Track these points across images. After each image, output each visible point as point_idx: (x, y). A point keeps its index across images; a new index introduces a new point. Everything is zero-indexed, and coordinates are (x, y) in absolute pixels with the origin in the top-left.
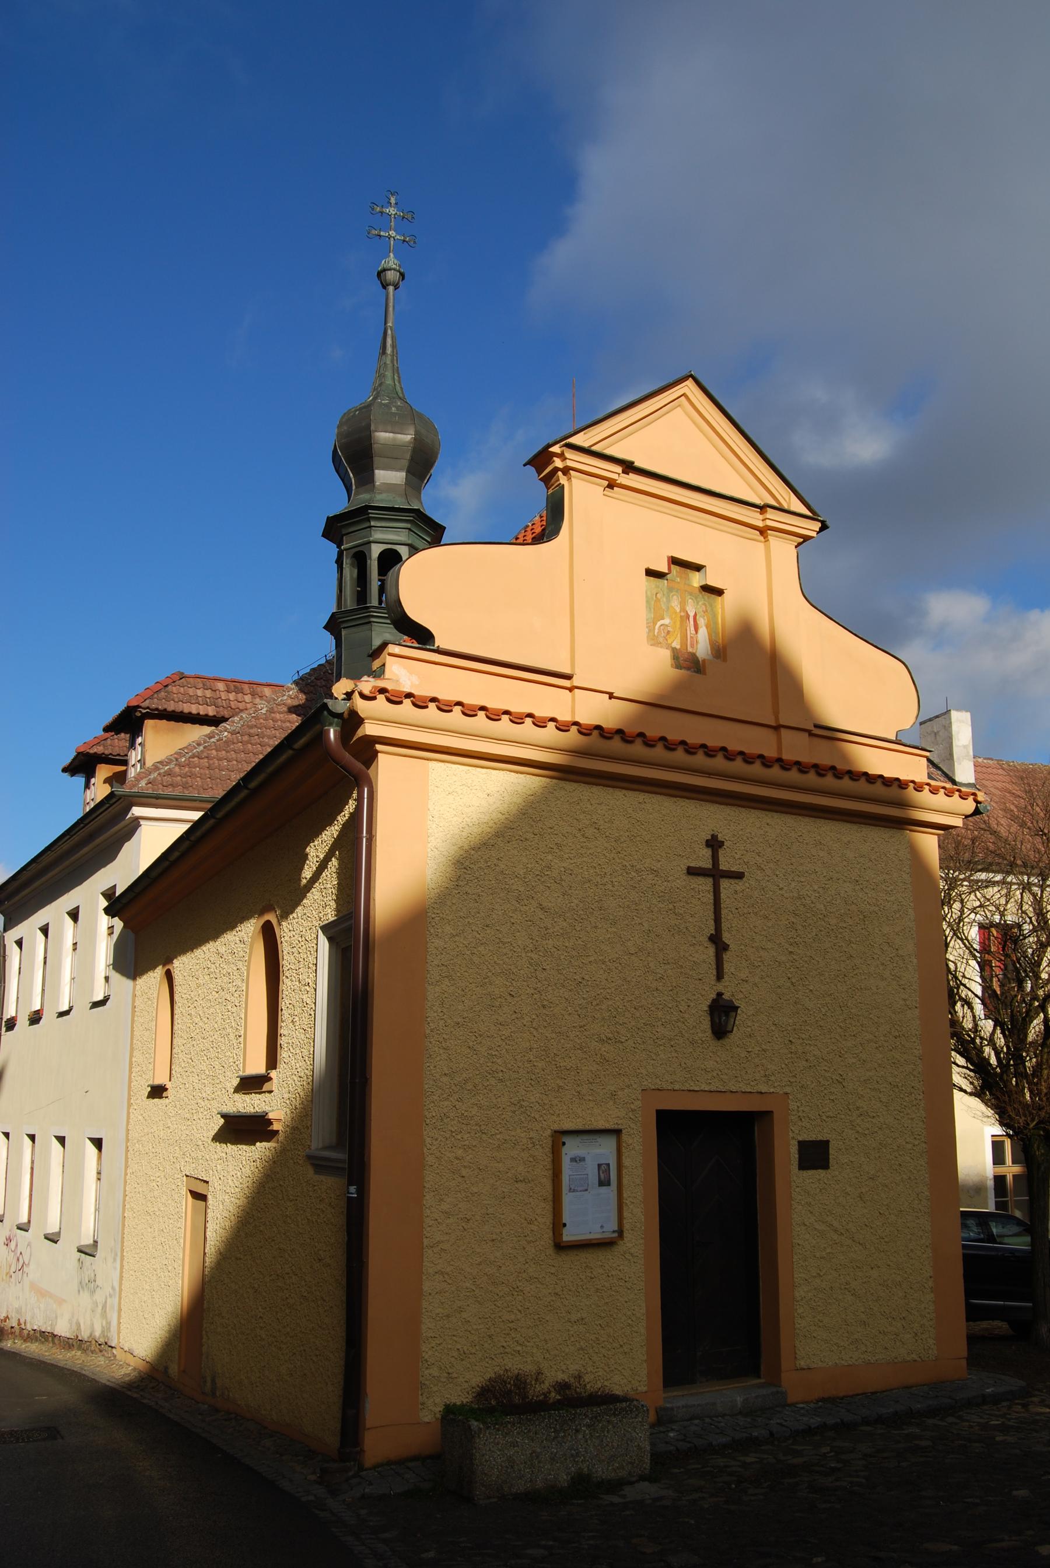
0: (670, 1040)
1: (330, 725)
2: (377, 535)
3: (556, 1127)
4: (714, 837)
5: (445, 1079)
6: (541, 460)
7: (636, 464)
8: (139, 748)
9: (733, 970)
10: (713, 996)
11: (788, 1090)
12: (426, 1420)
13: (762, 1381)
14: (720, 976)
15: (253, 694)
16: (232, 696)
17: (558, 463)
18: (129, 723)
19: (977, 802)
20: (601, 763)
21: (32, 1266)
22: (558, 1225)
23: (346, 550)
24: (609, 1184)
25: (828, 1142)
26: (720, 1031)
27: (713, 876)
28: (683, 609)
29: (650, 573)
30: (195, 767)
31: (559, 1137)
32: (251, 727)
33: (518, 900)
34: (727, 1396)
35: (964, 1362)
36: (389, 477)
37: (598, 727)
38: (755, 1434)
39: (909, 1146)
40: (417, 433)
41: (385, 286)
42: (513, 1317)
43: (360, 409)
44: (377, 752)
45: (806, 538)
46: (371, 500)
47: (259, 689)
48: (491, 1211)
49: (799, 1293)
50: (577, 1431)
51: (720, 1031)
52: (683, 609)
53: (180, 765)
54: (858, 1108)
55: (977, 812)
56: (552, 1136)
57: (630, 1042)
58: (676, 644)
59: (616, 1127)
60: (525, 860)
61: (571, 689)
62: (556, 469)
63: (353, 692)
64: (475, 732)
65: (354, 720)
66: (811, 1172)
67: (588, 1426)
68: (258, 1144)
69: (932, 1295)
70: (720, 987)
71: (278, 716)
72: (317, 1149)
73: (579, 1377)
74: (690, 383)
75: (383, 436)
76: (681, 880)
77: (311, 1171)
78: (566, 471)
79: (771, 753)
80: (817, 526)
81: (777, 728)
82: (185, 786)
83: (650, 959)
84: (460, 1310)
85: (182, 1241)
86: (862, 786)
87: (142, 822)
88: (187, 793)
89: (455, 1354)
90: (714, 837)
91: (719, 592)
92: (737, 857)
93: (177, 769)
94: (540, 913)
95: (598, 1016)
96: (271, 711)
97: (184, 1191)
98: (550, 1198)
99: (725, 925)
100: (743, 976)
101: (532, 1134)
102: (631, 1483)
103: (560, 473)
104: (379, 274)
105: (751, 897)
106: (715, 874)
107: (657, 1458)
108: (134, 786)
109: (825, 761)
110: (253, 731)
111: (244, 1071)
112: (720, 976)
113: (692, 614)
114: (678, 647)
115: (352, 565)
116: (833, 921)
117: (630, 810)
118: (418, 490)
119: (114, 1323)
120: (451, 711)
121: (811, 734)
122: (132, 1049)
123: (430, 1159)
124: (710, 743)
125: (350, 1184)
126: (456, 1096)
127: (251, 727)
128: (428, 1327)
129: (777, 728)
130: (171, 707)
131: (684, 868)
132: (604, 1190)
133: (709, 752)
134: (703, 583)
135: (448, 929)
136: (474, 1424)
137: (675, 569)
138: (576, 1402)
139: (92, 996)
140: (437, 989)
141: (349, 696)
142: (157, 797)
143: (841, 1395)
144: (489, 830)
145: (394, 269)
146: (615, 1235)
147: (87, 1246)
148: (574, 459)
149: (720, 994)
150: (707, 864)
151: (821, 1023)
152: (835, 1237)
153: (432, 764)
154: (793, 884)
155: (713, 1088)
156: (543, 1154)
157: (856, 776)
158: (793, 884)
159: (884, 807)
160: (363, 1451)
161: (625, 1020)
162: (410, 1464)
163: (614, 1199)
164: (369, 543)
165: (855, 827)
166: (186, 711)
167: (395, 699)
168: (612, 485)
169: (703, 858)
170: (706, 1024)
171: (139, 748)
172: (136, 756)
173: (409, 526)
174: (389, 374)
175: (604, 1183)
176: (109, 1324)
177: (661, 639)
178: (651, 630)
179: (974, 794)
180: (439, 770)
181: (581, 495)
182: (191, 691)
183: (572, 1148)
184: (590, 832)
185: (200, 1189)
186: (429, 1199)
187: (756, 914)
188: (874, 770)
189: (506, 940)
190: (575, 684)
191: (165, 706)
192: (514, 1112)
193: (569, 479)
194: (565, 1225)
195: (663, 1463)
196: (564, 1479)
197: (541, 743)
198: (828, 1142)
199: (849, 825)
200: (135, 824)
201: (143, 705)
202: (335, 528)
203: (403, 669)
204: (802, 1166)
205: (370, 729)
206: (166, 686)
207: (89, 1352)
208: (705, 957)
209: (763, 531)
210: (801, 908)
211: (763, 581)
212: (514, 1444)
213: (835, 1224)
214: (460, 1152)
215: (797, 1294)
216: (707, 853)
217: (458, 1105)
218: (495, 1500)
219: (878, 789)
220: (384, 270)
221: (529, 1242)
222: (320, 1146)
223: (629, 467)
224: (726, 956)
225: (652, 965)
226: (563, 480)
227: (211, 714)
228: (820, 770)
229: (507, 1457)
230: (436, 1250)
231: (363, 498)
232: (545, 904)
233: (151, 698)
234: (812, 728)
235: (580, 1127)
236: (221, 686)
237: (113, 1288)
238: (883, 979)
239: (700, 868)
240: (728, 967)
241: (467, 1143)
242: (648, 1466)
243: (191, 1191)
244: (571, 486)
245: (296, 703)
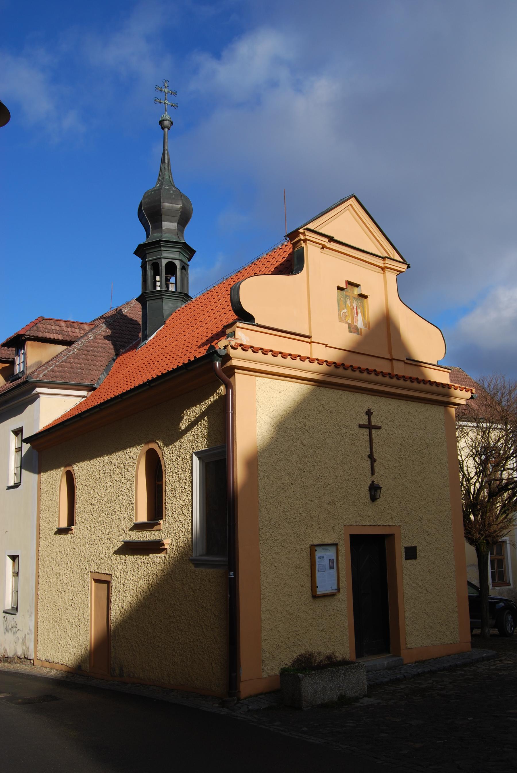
0: (354, 502)
1: (217, 360)
2: (164, 255)
3: (311, 543)
4: (369, 410)
5: (267, 523)
6: (293, 235)
7: (335, 238)
8: (22, 356)
9: (378, 471)
10: (370, 482)
11: (400, 524)
12: (265, 676)
13: (390, 655)
14: (373, 473)
15: (80, 329)
16: (69, 329)
17: (302, 237)
18: (17, 342)
19: (472, 393)
20: (340, 378)
22: (314, 586)
23: (148, 261)
24: (333, 568)
25: (416, 547)
26: (374, 498)
27: (369, 428)
28: (352, 305)
29: (339, 288)
30: (65, 367)
31: (313, 548)
32: (87, 347)
34: (380, 661)
35: (470, 644)
36: (169, 225)
37: (334, 363)
38: (398, 677)
39: (447, 548)
40: (183, 204)
41: (163, 128)
42: (297, 629)
43: (154, 191)
44: (235, 373)
45: (401, 272)
46: (161, 237)
47: (82, 326)
48: (287, 581)
50: (340, 676)
51: (374, 498)
52: (352, 305)
53: (56, 366)
54: (427, 532)
55: (472, 398)
56: (310, 547)
57: (339, 504)
58: (349, 321)
59: (334, 542)
60: (295, 422)
61: (310, 343)
62: (301, 240)
63: (228, 345)
64: (241, 358)
65: (227, 358)
66: (410, 561)
67: (344, 674)
68: (151, 555)
69: (457, 614)
70: (373, 479)
71: (99, 341)
72: (196, 556)
73: (333, 653)
74: (353, 199)
75: (166, 205)
76: (356, 430)
77: (193, 567)
78: (305, 241)
79: (387, 370)
80: (405, 266)
81: (391, 360)
82: (62, 377)
83: (345, 466)
84: (276, 627)
85: (89, 604)
86: (427, 387)
87: (40, 395)
88: (63, 381)
89: (275, 646)
90: (369, 410)
91: (366, 297)
92: (378, 419)
93: (56, 368)
94: (302, 446)
95: (326, 492)
96: (95, 338)
98: (310, 575)
99: (374, 450)
100: (382, 473)
101: (302, 547)
102: (361, 698)
103: (302, 241)
104: (160, 122)
105: (384, 437)
106: (370, 427)
107: (370, 687)
108: (37, 377)
109: (414, 376)
110: (88, 349)
111: (136, 520)
112: (373, 473)
113: (355, 307)
114: (350, 323)
115: (151, 269)
116: (416, 448)
117: (336, 398)
118: (182, 232)
120: (267, 354)
121: (405, 363)
122: (39, 509)
123: (262, 559)
124: (274, 349)
125: (230, 571)
126: (271, 530)
127: (87, 347)
128: (264, 635)
129: (391, 360)
130: (40, 335)
131: (358, 424)
132: (332, 571)
133: (369, 371)
134: (360, 293)
136: (300, 675)
137: (348, 286)
138: (332, 664)
139: (8, 483)
140: (263, 482)
141: (226, 347)
142: (50, 383)
143: (424, 659)
144: (281, 408)
145: (168, 120)
146: (337, 591)
147: (9, 610)
148: (309, 235)
149: (373, 482)
150: (366, 423)
151: (412, 494)
152: (420, 589)
153: (258, 379)
154: (400, 431)
155: (372, 524)
156: (306, 555)
157: (432, 383)
158: (400, 431)
159: (438, 397)
160: (240, 692)
161: (337, 494)
162: (261, 696)
163: (334, 575)
164: (161, 258)
165: (423, 405)
166: (48, 337)
167: (245, 348)
168: (324, 247)
170: (368, 495)
171: (22, 356)
172: (20, 360)
173: (179, 250)
174: (167, 173)
175: (331, 568)
176: (28, 648)
177: (343, 319)
178: (339, 315)
179: (471, 390)
180: (261, 381)
181: (312, 253)
182: (49, 327)
183: (319, 553)
184: (320, 408)
187: (386, 445)
188: (438, 381)
189: (289, 459)
190: (313, 341)
191: (37, 335)
192: (294, 537)
193: (306, 244)
194: (317, 587)
195: (373, 688)
196: (335, 697)
197: (312, 371)
198: (416, 547)
199: (420, 404)
200: (37, 396)
201: (26, 334)
202: (141, 251)
203: (243, 334)
204: (407, 558)
205: (235, 362)
206: (36, 324)
208: (366, 465)
209: (383, 269)
210: (403, 442)
211: (381, 291)
212: (316, 683)
213: (420, 584)
214: (274, 555)
215: (406, 615)
216: (366, 417)
217: (273, 534)
218: (310, 708)
219: (434, 388)
220: (163, 120)
221: (302, 595)
222: (198, 555)
223: (331, 239)
224: (376, 464)
225: (346, 469)
226: (303, 245)
227: (60, 339)
228: (412, 379)
229: (315, 689)
230: (266, 600)
231: (155, 236)
232: (304, 442)
233: (30, 330)
234: (405, 360)
235: (320, 543)
236: (63, 324)
237: (30, 630)
238: (436, 473)
239: (364, 424)
240: (376, 470)
241: (277, 551)
242: (366, 691)
243: (94, 579)
244: (307, 248)
245: (106, 334)
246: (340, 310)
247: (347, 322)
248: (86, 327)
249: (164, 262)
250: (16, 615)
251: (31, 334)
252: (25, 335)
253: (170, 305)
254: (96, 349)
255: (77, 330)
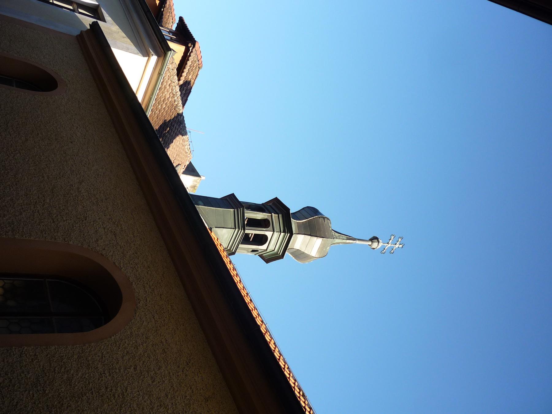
2: (276, 234)
23: (272, 216)
87: (147, 58)
164: (274, 231)
200: (146, 54)
201: (194, 50)
249: (269, 234)
251: (192, 54)
252: (193, 48)
253: (226, 236)
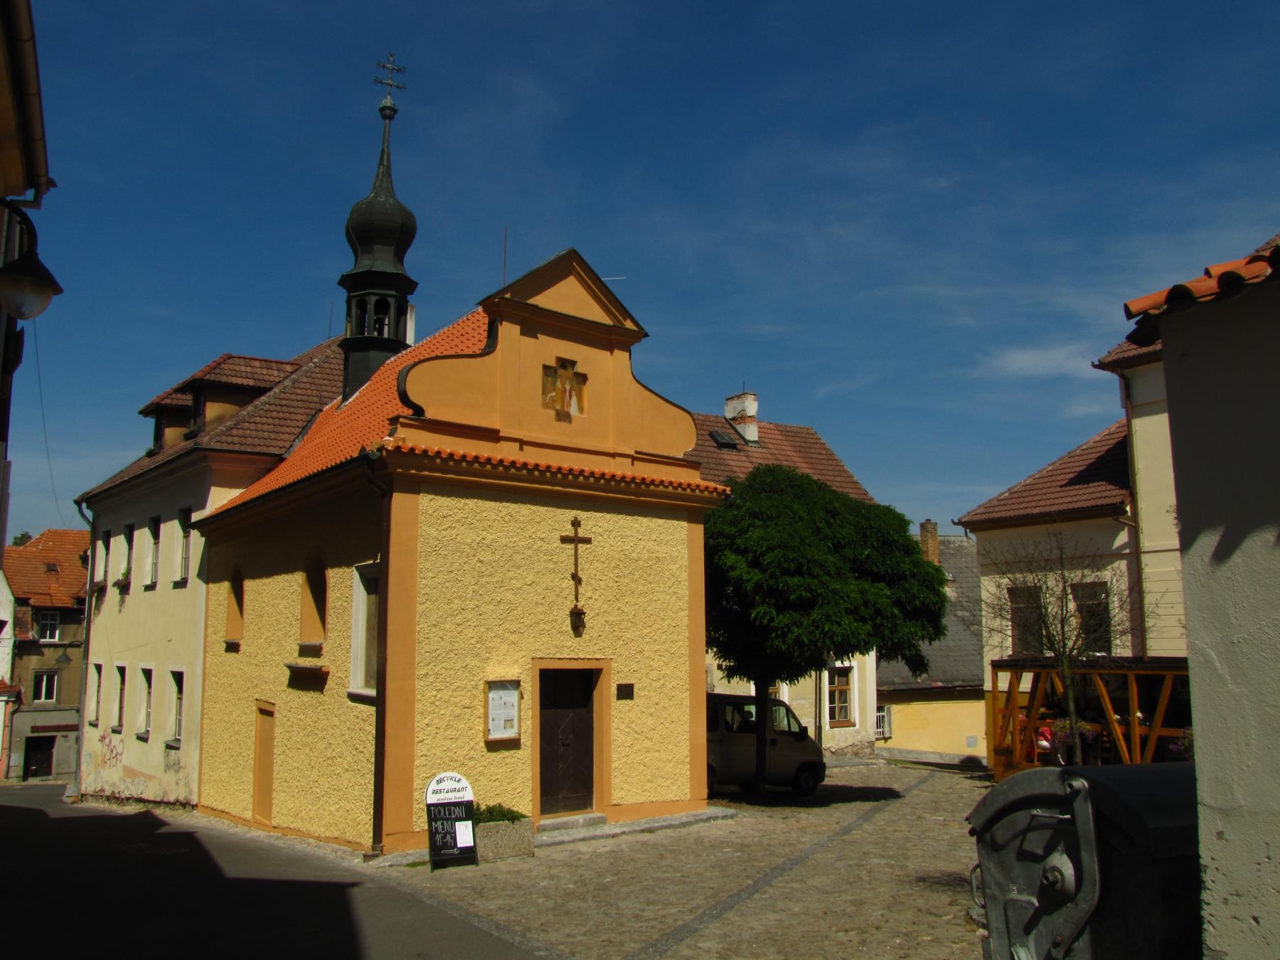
21: (124, 755)
33: (467, 556)
49: (614, 765)
58: (558, 407)
97: (254, 708)
112: (577, 599)
119: (195, 789)
135: (430, 574)
163: (518, 715)
169: (569, 531)
176: (191, 792)
178: (544, 400)
182: (237, 368)
184: (507, 518)
185: (269, 708)
186: (418, 718)
202: (348, 282)
207: (1010, 855)
236: (257, 364)
246: (545, 392)
247: (554, 409)
248: (289, 368)
250: (178, 749)
254: (307, 386)
255: (275, 373)
